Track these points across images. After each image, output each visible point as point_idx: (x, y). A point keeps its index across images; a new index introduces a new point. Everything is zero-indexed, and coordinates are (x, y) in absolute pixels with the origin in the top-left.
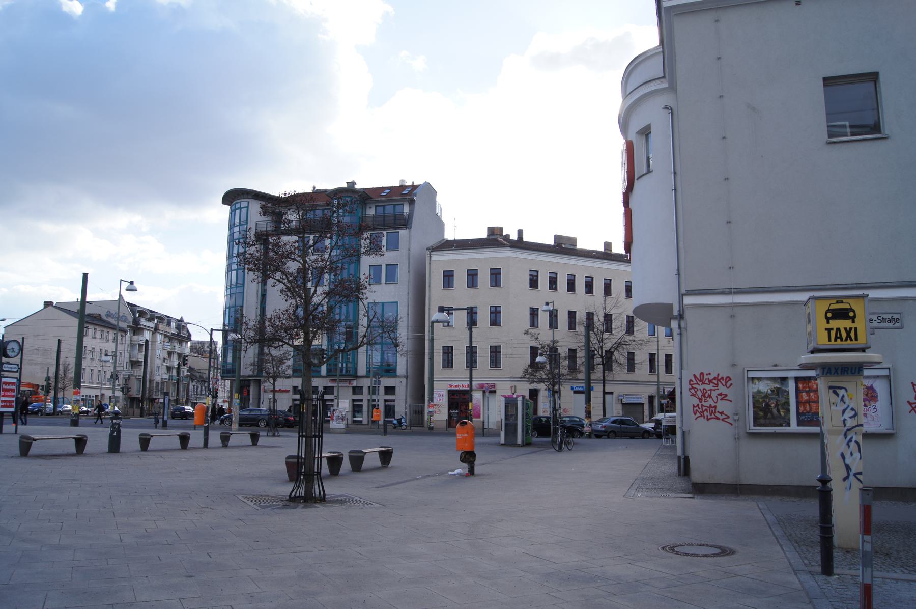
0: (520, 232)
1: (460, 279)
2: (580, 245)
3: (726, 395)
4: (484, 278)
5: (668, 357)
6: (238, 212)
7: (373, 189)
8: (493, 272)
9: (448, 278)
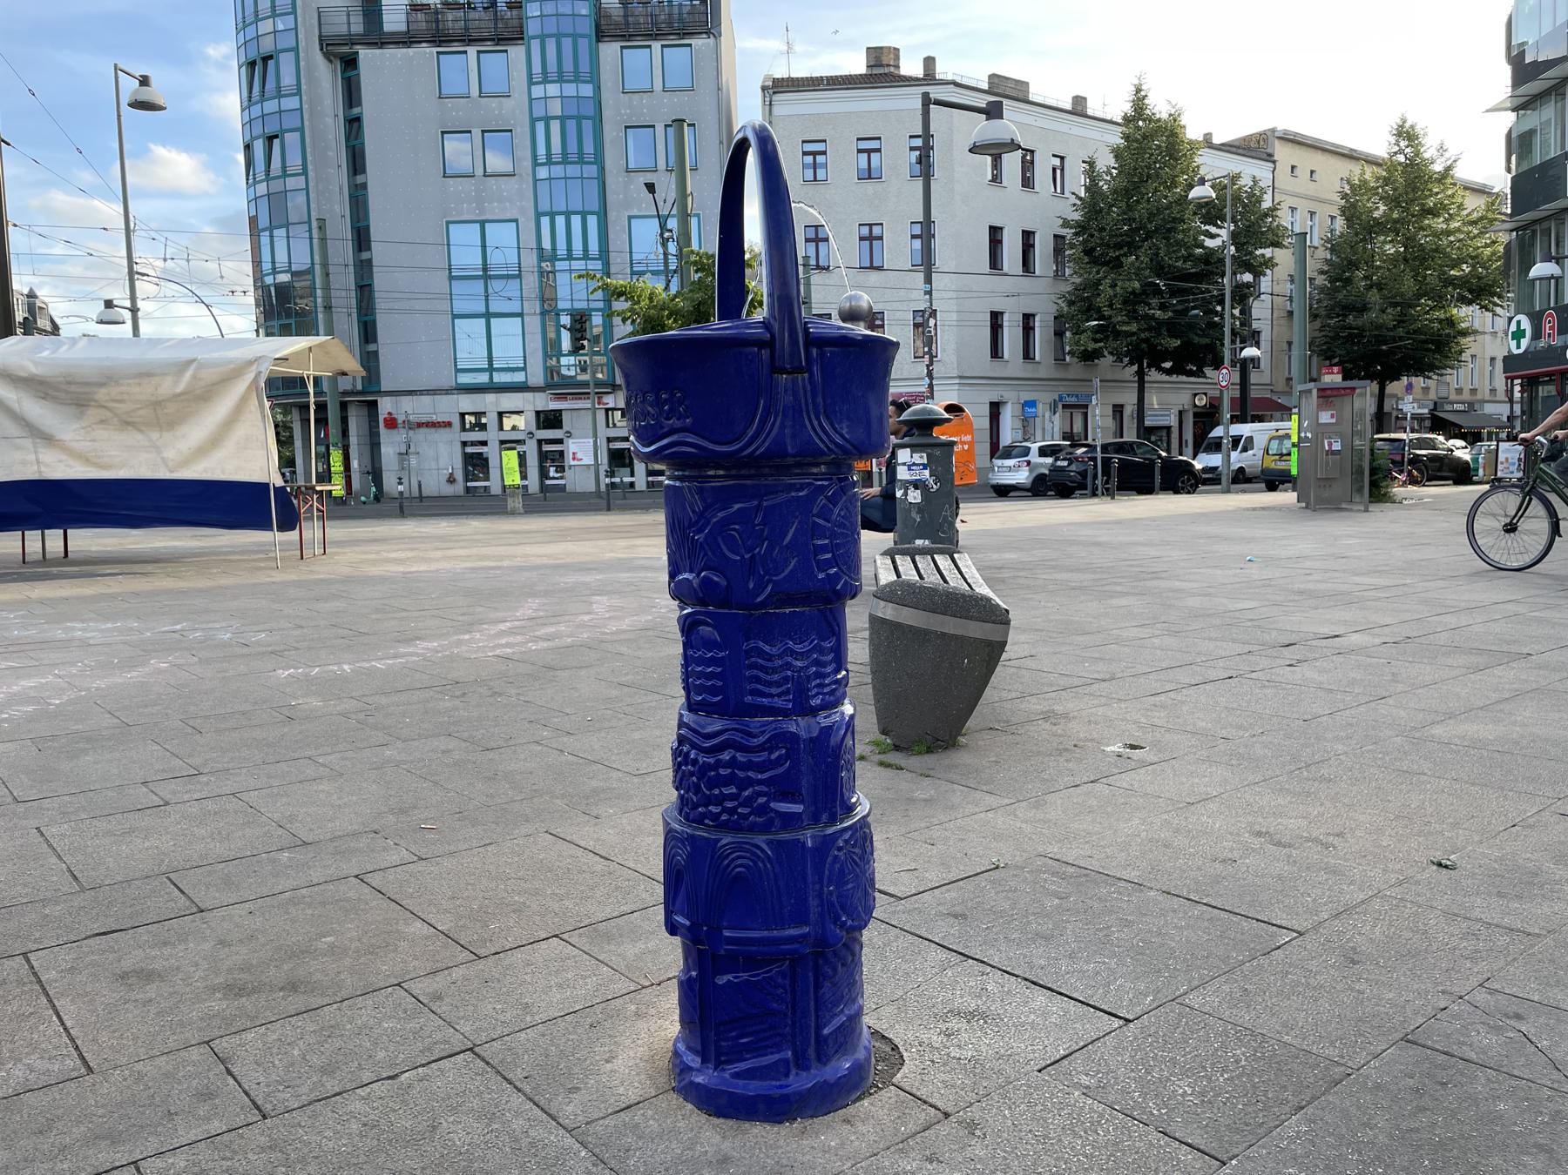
0: (929, 62)
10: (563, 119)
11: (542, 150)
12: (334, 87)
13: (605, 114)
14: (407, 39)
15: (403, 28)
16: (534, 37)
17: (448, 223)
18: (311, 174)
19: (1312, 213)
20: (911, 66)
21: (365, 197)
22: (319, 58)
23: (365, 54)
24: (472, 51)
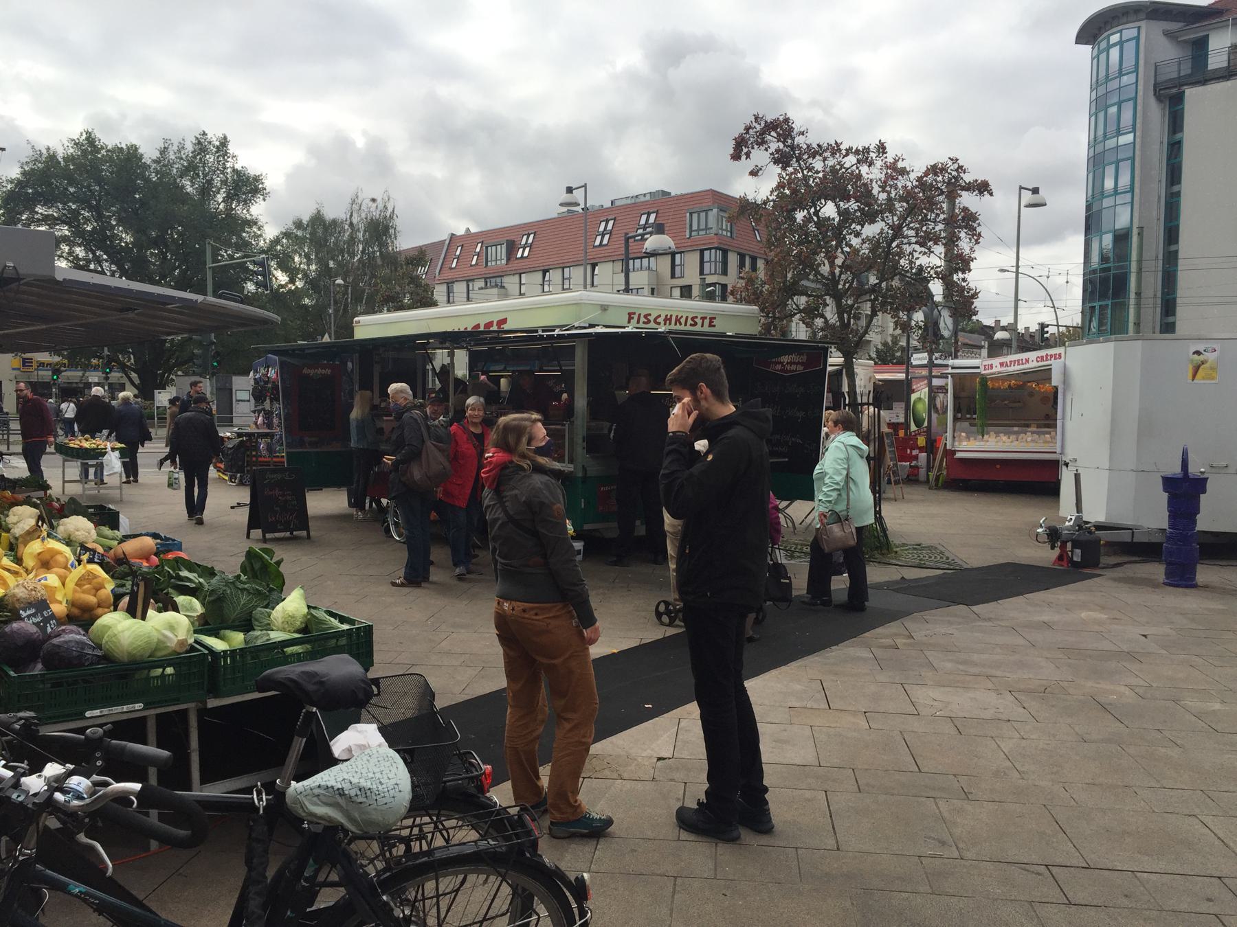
6: (1103, 57)
12: (1163, 123)
18: (1137, 190)
21: (1178, 204)
22: (1152, 101)
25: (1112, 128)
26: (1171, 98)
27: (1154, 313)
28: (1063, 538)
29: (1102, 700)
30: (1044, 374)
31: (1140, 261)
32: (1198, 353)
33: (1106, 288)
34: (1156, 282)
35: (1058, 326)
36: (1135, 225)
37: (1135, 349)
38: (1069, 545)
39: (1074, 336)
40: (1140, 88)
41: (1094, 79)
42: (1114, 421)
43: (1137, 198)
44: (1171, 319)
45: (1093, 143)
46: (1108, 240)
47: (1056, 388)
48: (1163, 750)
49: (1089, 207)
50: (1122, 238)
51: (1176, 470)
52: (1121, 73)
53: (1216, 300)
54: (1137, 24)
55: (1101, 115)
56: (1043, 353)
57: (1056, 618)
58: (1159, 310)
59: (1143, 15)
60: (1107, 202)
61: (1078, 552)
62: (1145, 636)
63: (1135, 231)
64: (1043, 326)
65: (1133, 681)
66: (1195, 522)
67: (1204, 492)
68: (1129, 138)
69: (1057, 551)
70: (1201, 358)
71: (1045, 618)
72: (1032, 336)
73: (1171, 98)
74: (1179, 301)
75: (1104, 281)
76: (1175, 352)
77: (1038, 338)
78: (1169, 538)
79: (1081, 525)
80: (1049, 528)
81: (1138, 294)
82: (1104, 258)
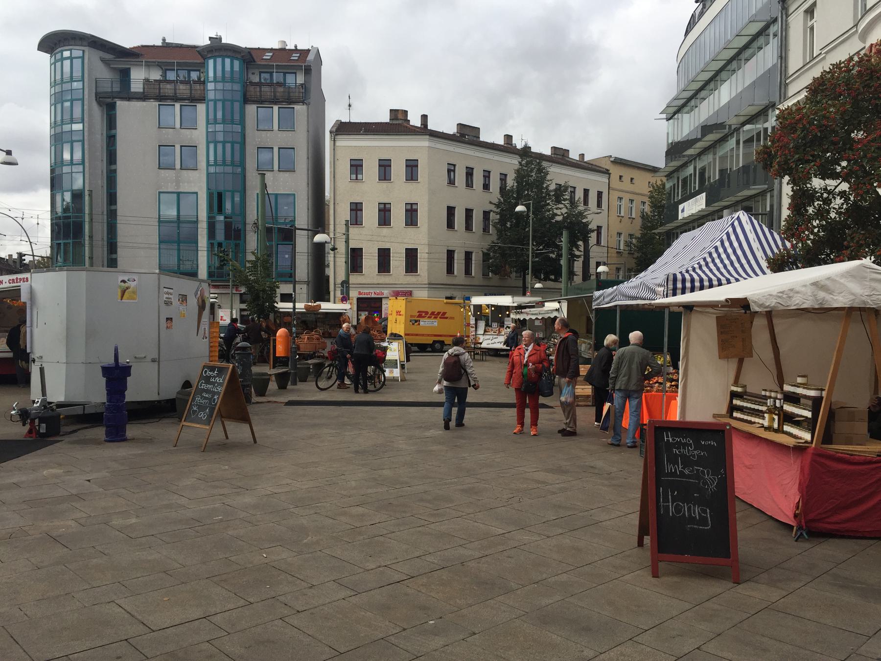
0: (424, 118)
1: (371, 170)
2: (484, 137)
3: (444, 313)
4: (398, 170)
5: (600, 194)
6: (59, 64)
7: (134, 48)
8: (354, 163)
9: (356, 167)
10: (224, 143)
11: (212, 158)
12: (103, 120)
13: (248, 140)
14: (143, 97)
15: (142, 90)
16: (212, 100)
17: (160, 193)
18: (87, 164)
19: (632, 201)
20: (415, 121)
22: (95, 104)
23: (120, 104)
24: (177, 106)
25: (67, 117)
26: (107, 104)
27: (103, 251)
28: (32, 417)
29: (54, 534)
30: (15, 293)
31: (91, 214)
32: (124, 281)
33: (67, 228)
34: (103, 231)
35: (33, 256)
36: (87, 189)
37: (81, 276)
38: (37, 421)
39: (44, 265)
40: (86, 93)
41: (53, 80)
42: (68, 329)
43: (87, 169)
44: (114, 256)
45: (54, 125)
46: (68, 197)
47: (25, 303)
48: (95, 560)
49: (52, 171)
50: (77, 196)
51: (110, 361)
52: (72, 79)
53: (143, 245)
54: (83, 48)
55: (59, 106)
56: (14, 277)
57: (24, 478)
58: (106, 249)
59: (85, 43)
60: (66, 169)
61: (44, 425)
62: (89, 481)
63: (87, 193)
64: (21, 255)
65: (79, 515)
66: (124, 397)
67: (130, 375)
68: (77, 127)
69: (28, 427)
70: (126, 285)
71: (15, 480)
72: (14, 261)
73: (107, 104)
74: (119, 244)
75: (67, 226)
76: (114, 279)
77: (18, 266)
78: (107, 409)
79: (46, 405)
80: (20, 410)
81: (91, 237)
82: (66, 210)
